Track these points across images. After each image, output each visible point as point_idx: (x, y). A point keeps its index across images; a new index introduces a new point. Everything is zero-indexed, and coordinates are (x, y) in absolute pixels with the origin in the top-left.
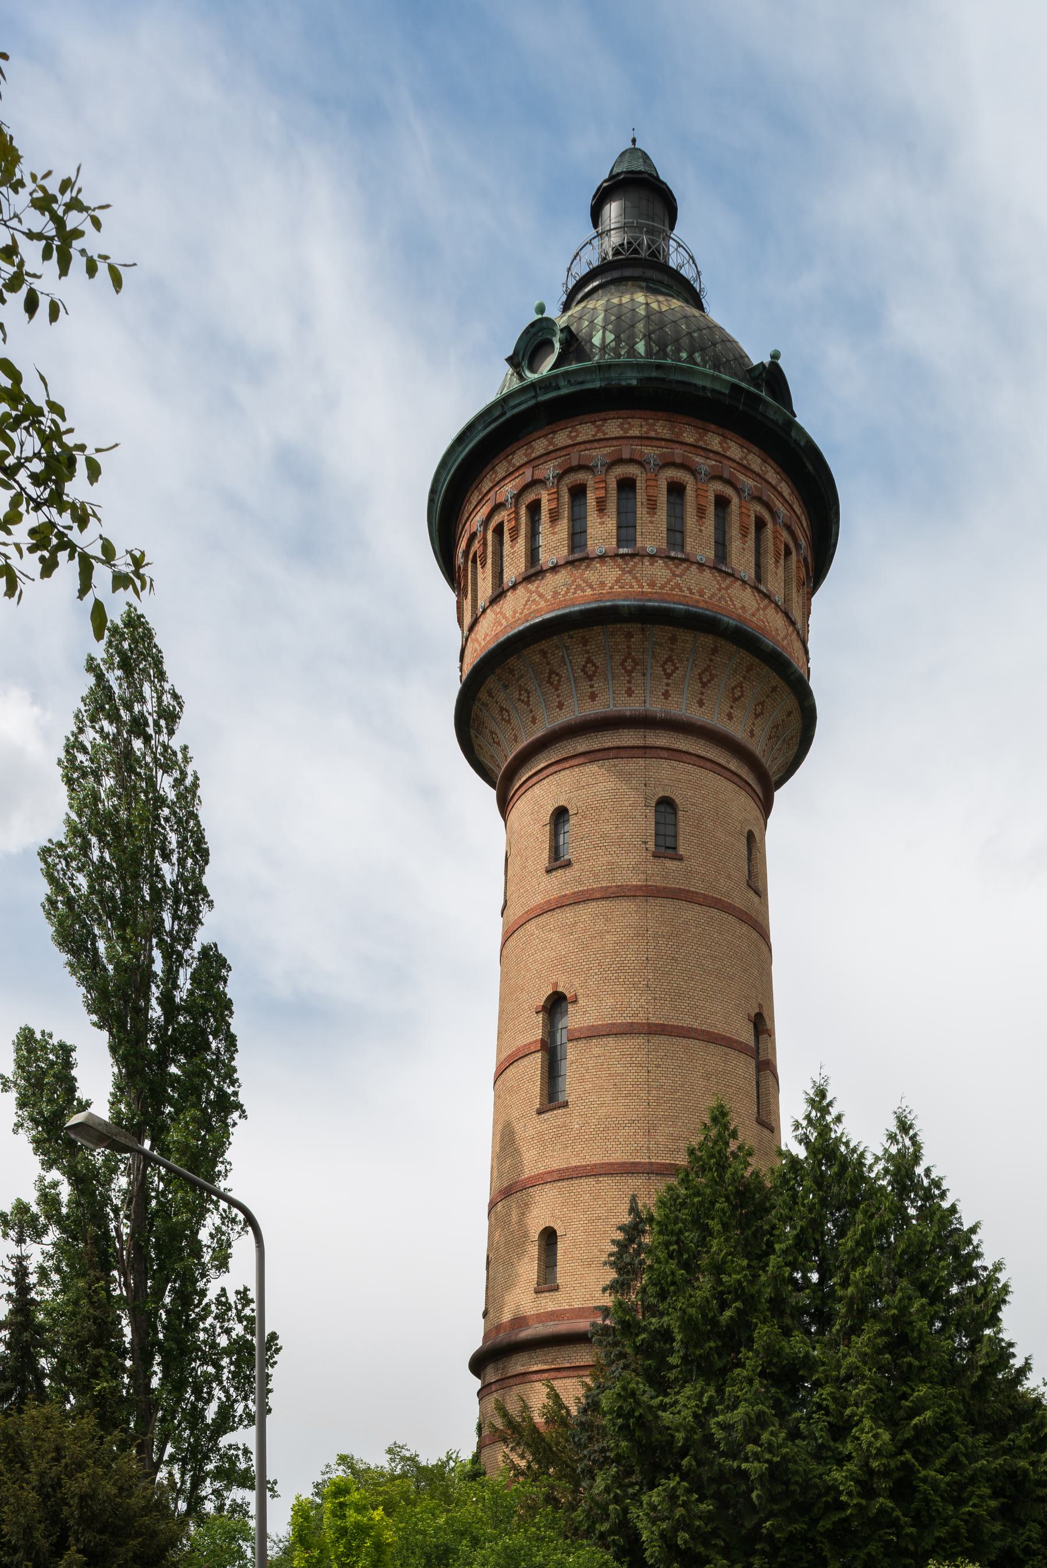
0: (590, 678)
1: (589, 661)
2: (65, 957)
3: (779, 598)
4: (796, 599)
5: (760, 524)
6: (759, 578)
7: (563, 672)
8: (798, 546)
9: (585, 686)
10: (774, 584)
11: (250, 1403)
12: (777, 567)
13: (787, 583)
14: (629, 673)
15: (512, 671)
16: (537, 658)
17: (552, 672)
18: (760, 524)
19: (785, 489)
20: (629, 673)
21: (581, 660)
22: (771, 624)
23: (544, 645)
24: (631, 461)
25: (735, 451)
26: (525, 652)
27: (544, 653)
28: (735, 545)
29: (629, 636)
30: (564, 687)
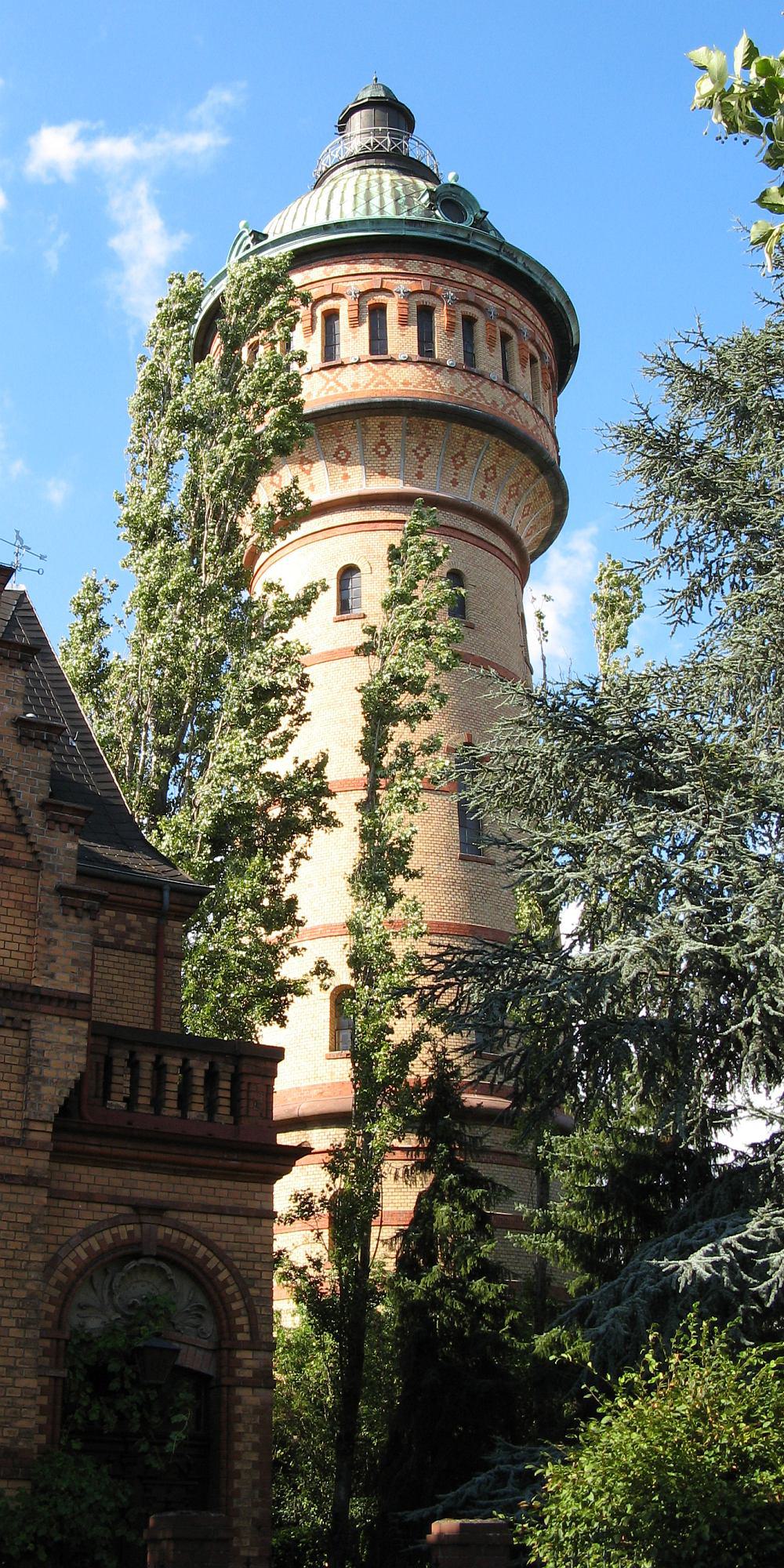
0: (487, 480)
1: (493, 468)
2: (364, 723)
3: (529, 397)
4: (545, 399)
5: (505, 338)
6: (506, 376)
7: (471, 461)
8: (541, 352)
9: (481, 482)
10: (522, 379)
11: (192, 941)
12: (523, 367)
13: (534, 385)
14: (511, 496)
15: (427, 428)
16: (459, 436)
17: (461, 454)
18: (505, 338)
19: (529, 313)
20: (511, 496)
21: (489, 463)
22: (524, 419)
23: (474, 433)
24: (325, 298)
25: (514, 301)
26: (454, 425)
27: (468, 438)
28: (481, 348)
29: (528, 472)
30: (463, 472)
